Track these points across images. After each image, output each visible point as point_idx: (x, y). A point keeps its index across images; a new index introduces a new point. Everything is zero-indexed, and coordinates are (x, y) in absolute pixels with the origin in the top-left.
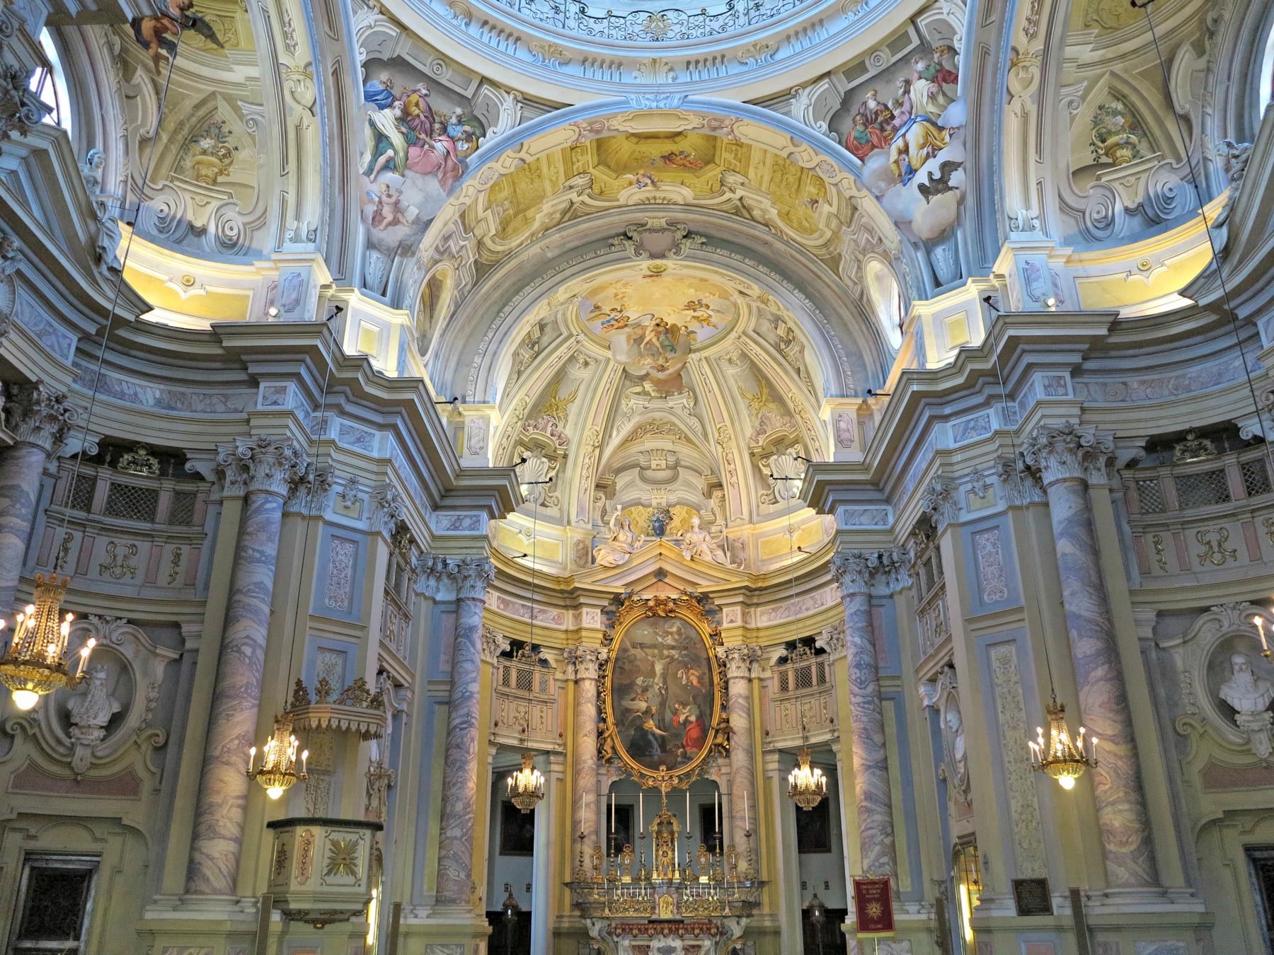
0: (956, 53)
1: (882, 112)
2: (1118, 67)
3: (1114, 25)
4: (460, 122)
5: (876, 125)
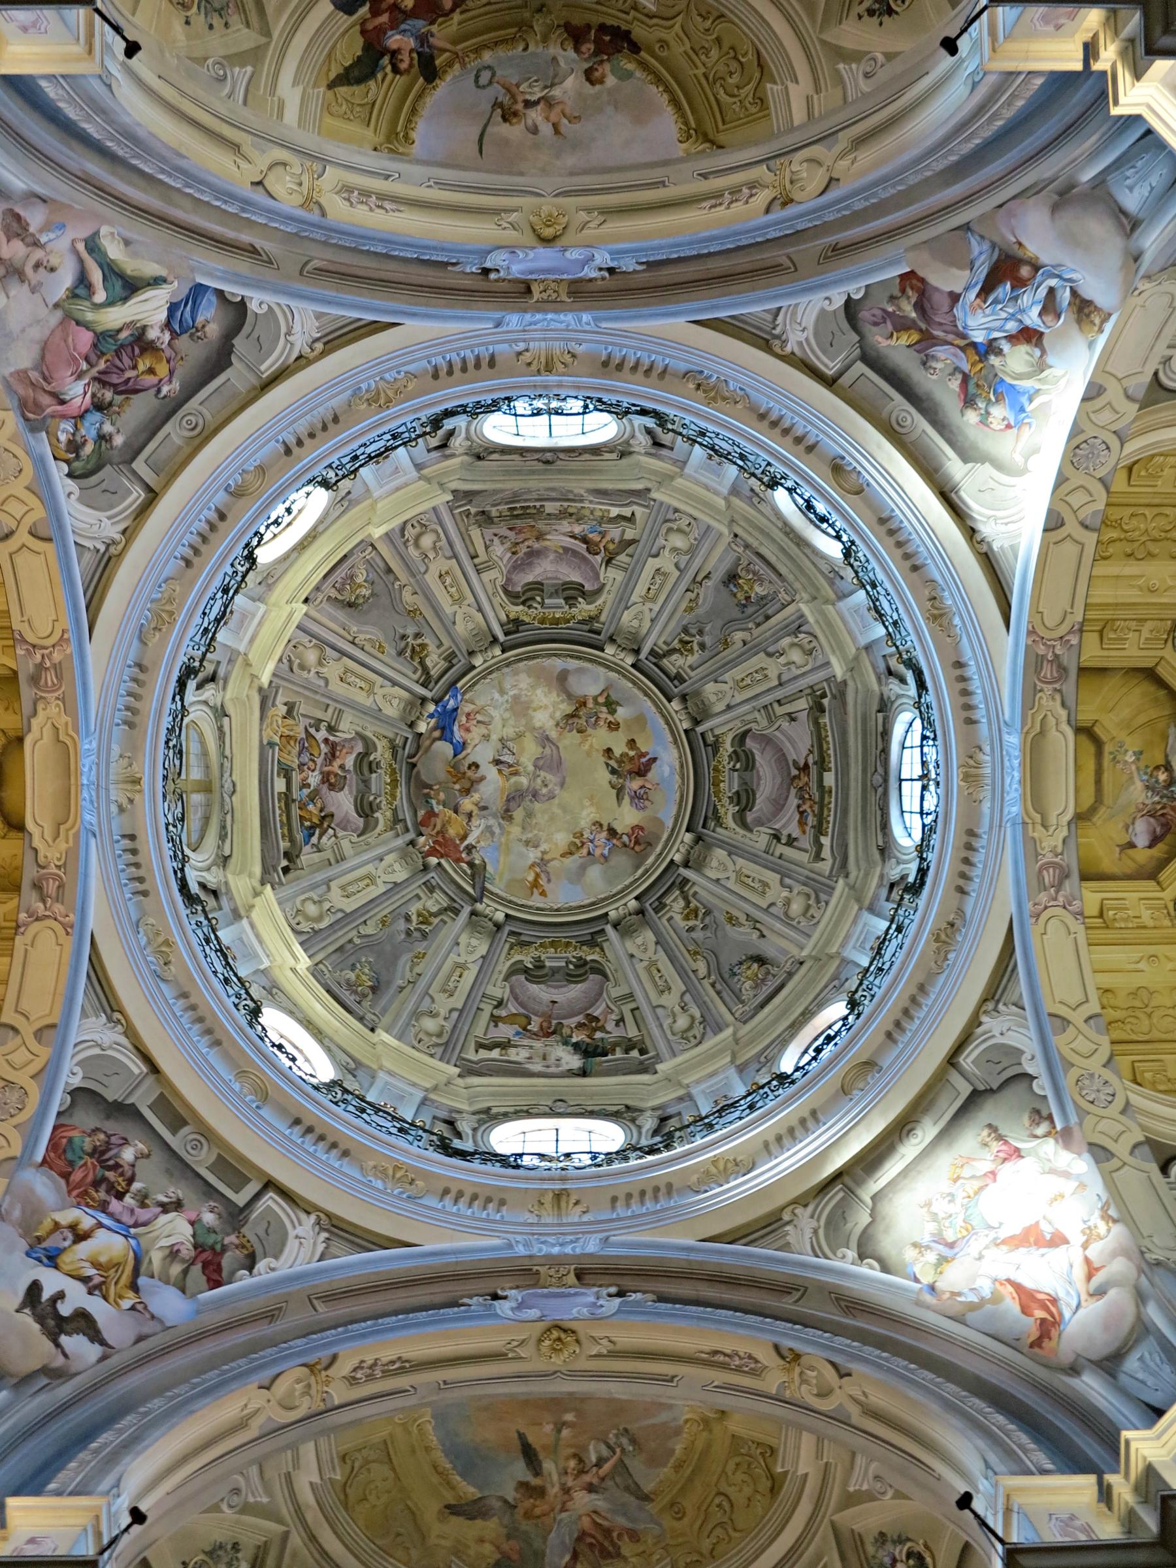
0: (250, 1268)
1: (122, 1175)
2: (296, 1540)
3: (352, 1498)
4: (102, 438)
5: (100, 1172)
